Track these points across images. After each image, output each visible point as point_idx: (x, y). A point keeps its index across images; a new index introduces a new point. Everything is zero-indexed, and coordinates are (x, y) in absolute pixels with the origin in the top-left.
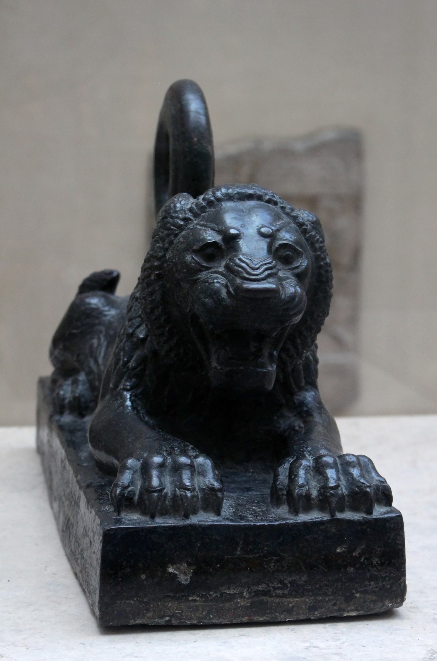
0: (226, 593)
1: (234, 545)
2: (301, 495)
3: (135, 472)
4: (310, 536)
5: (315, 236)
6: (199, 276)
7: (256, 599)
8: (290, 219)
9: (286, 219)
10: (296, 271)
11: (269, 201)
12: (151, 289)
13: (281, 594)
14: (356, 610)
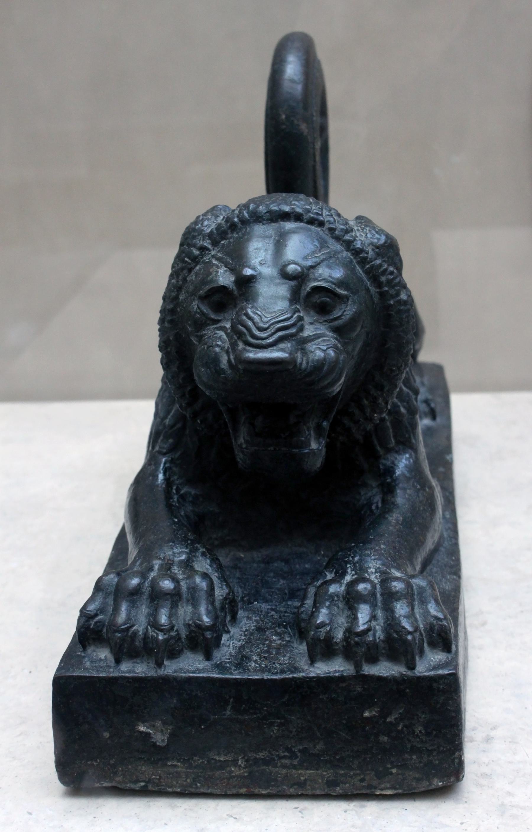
0: (215, 759)
1: (222, 704)
2: (319, 640)
4: (327, 696)
6: (204, 332)
8: (342, 245)
10: (336, 323)
11: (311, 222)
13: (288, 765)
14: (393, 788)
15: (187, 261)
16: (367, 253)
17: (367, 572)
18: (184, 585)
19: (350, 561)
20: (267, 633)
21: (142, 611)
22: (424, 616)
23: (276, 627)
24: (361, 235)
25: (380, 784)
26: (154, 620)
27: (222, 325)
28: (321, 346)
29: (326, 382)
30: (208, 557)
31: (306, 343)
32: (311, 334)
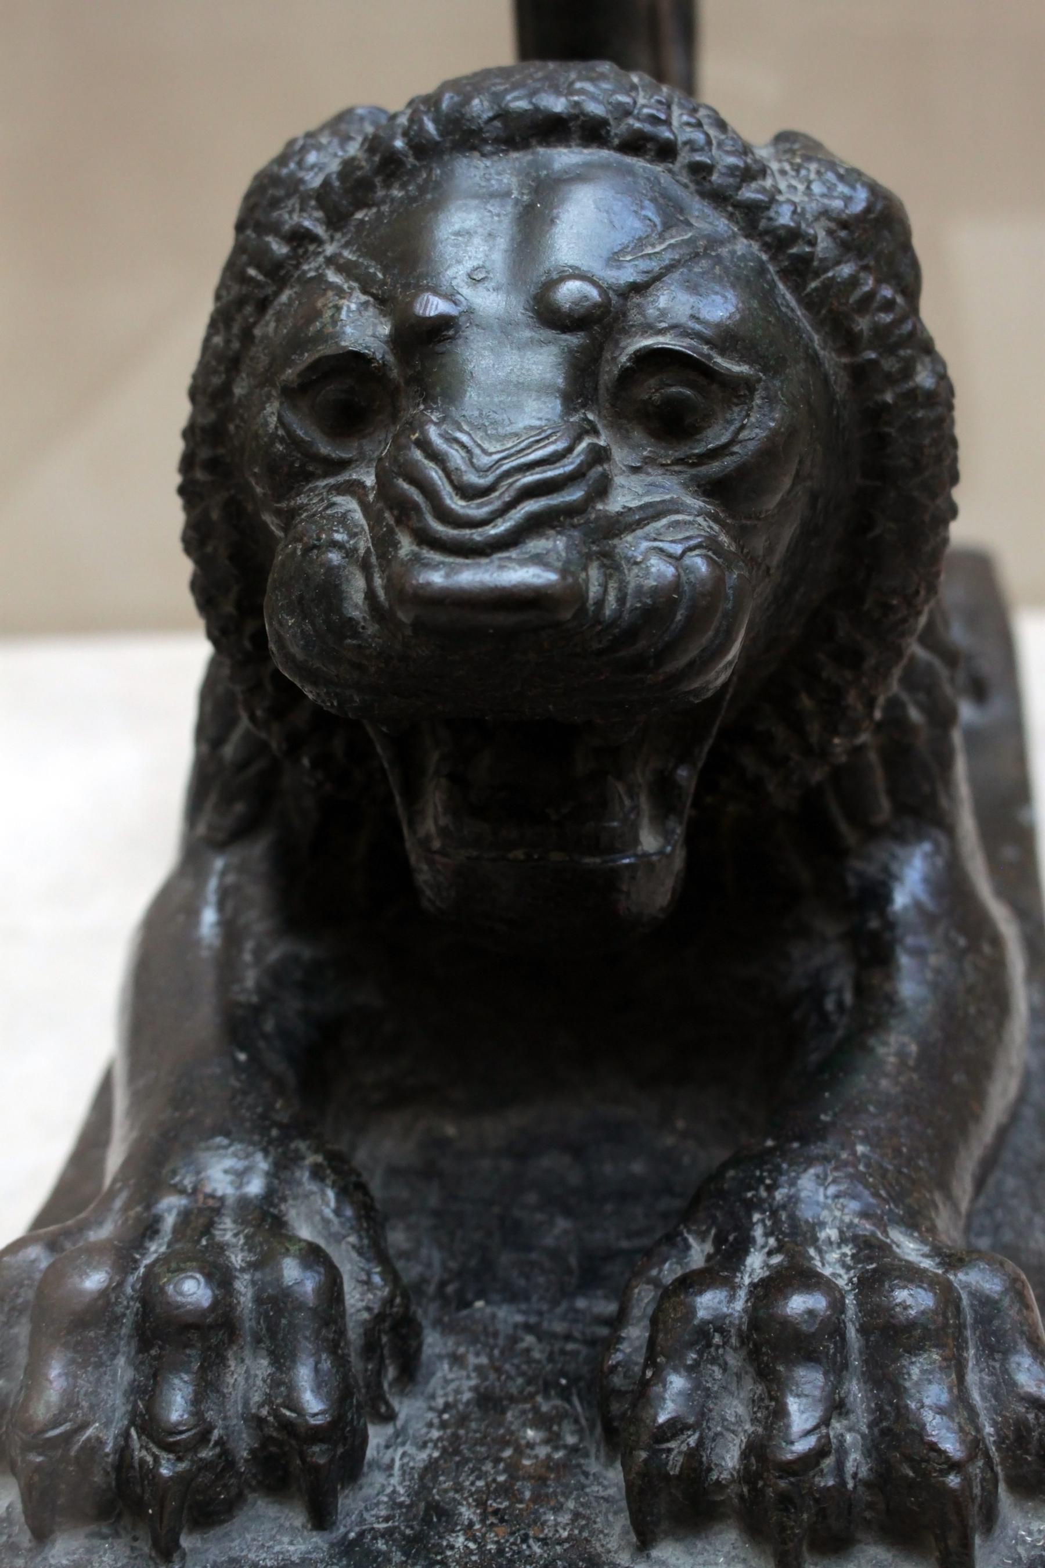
2: (667, 1477)
8: (731, 217)
10: (715, 467)
11: (635, 145)
15: (251, 279)
16: (812, 242)
17: (814, 1241)
18: (244, 1288)
19: (762, 1201)
20: (509, 1415)
21: (114, 1375)
22: (996, 1396)
23: (537, 1393)
24: (792, 188)
26: (148, 1408)
27: (354, 476)
28: (666, 539)
29: (683, 661)
30: (329, 1182)
31: (618, 535)
32: (633, 504)
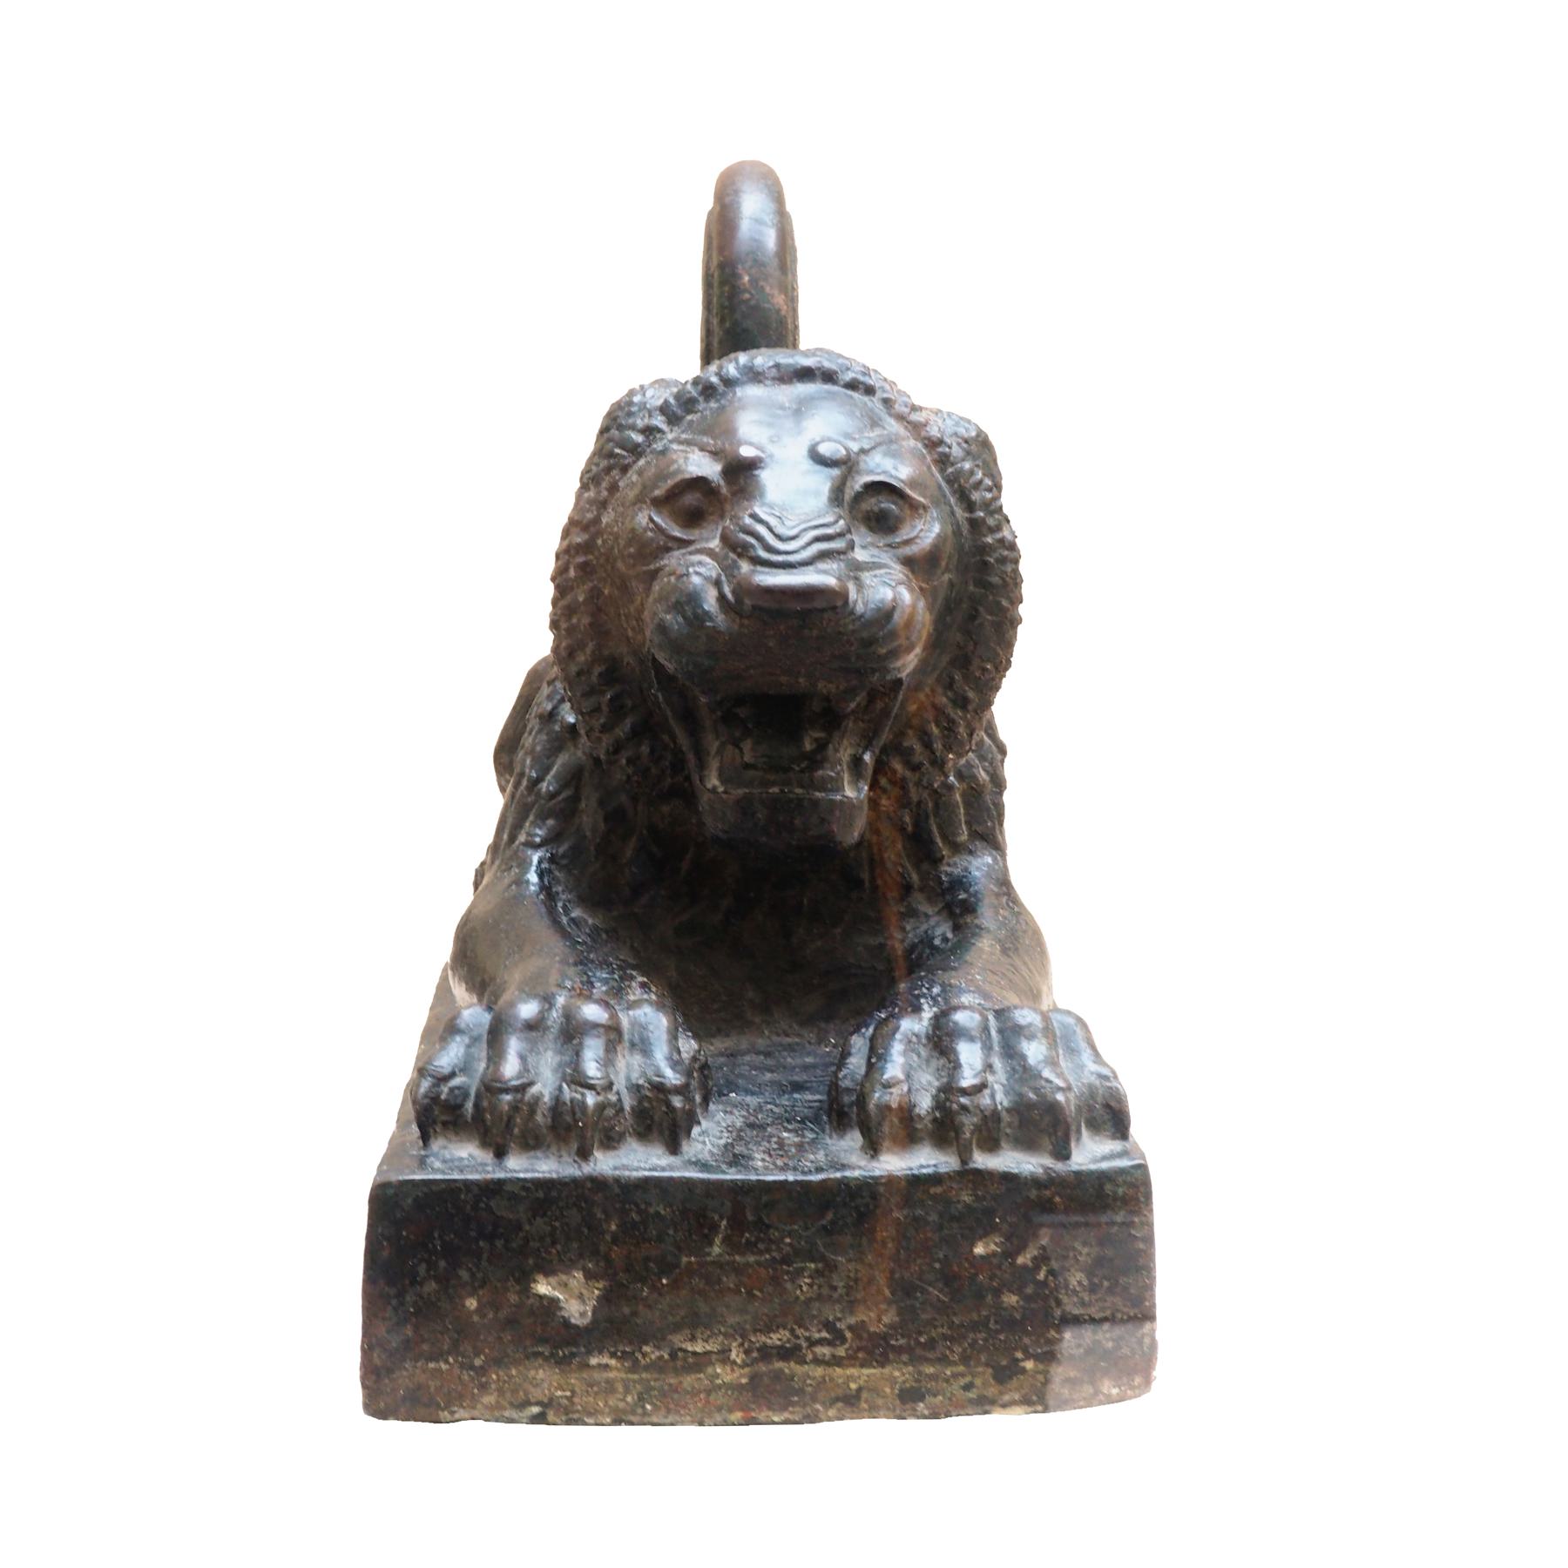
0: (685, 1351)
2: (888, 1107)
3: (475, 1040)
5: (972, 473)
7: (763, 1368)
9: (893, 426)
10: (908, 551)
11: (853, 385)
12: (569, 598)
25: (1001, 1393)
